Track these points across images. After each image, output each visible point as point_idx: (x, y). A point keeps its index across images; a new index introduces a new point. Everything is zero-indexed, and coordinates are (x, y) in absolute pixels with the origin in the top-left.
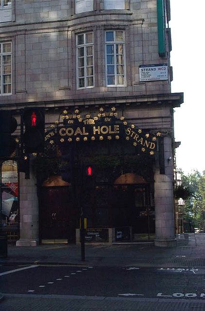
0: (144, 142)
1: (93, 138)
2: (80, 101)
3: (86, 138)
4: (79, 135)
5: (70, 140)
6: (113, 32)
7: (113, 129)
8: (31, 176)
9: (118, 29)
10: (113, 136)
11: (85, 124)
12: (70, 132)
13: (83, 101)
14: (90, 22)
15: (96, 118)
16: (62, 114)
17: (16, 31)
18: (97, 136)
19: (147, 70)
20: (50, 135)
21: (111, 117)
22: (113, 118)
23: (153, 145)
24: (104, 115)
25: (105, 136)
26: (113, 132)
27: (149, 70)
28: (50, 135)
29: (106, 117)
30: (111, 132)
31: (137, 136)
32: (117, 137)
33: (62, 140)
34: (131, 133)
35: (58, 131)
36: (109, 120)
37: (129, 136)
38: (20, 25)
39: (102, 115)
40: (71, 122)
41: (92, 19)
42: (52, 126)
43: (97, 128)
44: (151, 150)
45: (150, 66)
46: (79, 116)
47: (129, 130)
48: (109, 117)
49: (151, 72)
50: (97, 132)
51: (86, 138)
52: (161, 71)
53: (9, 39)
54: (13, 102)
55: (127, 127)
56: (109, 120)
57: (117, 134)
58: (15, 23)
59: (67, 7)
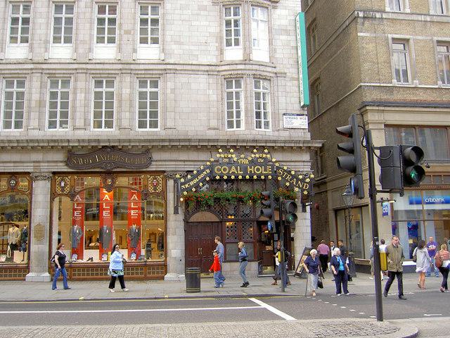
0: (297, 182)
2: (233, 141)
4: (233, 173)
14: (241, 70)
15: (250, 159)
17: (165, 70)
22: (265, 159)
24: (257, 156)
34: (284, 174)
36: (262, 161)
42: (208, 163)
45: (293, 115)
49: (294, 121)
54: (183, 138)
55: (278, 168)
56: (262, 161)
59: (216, 53)
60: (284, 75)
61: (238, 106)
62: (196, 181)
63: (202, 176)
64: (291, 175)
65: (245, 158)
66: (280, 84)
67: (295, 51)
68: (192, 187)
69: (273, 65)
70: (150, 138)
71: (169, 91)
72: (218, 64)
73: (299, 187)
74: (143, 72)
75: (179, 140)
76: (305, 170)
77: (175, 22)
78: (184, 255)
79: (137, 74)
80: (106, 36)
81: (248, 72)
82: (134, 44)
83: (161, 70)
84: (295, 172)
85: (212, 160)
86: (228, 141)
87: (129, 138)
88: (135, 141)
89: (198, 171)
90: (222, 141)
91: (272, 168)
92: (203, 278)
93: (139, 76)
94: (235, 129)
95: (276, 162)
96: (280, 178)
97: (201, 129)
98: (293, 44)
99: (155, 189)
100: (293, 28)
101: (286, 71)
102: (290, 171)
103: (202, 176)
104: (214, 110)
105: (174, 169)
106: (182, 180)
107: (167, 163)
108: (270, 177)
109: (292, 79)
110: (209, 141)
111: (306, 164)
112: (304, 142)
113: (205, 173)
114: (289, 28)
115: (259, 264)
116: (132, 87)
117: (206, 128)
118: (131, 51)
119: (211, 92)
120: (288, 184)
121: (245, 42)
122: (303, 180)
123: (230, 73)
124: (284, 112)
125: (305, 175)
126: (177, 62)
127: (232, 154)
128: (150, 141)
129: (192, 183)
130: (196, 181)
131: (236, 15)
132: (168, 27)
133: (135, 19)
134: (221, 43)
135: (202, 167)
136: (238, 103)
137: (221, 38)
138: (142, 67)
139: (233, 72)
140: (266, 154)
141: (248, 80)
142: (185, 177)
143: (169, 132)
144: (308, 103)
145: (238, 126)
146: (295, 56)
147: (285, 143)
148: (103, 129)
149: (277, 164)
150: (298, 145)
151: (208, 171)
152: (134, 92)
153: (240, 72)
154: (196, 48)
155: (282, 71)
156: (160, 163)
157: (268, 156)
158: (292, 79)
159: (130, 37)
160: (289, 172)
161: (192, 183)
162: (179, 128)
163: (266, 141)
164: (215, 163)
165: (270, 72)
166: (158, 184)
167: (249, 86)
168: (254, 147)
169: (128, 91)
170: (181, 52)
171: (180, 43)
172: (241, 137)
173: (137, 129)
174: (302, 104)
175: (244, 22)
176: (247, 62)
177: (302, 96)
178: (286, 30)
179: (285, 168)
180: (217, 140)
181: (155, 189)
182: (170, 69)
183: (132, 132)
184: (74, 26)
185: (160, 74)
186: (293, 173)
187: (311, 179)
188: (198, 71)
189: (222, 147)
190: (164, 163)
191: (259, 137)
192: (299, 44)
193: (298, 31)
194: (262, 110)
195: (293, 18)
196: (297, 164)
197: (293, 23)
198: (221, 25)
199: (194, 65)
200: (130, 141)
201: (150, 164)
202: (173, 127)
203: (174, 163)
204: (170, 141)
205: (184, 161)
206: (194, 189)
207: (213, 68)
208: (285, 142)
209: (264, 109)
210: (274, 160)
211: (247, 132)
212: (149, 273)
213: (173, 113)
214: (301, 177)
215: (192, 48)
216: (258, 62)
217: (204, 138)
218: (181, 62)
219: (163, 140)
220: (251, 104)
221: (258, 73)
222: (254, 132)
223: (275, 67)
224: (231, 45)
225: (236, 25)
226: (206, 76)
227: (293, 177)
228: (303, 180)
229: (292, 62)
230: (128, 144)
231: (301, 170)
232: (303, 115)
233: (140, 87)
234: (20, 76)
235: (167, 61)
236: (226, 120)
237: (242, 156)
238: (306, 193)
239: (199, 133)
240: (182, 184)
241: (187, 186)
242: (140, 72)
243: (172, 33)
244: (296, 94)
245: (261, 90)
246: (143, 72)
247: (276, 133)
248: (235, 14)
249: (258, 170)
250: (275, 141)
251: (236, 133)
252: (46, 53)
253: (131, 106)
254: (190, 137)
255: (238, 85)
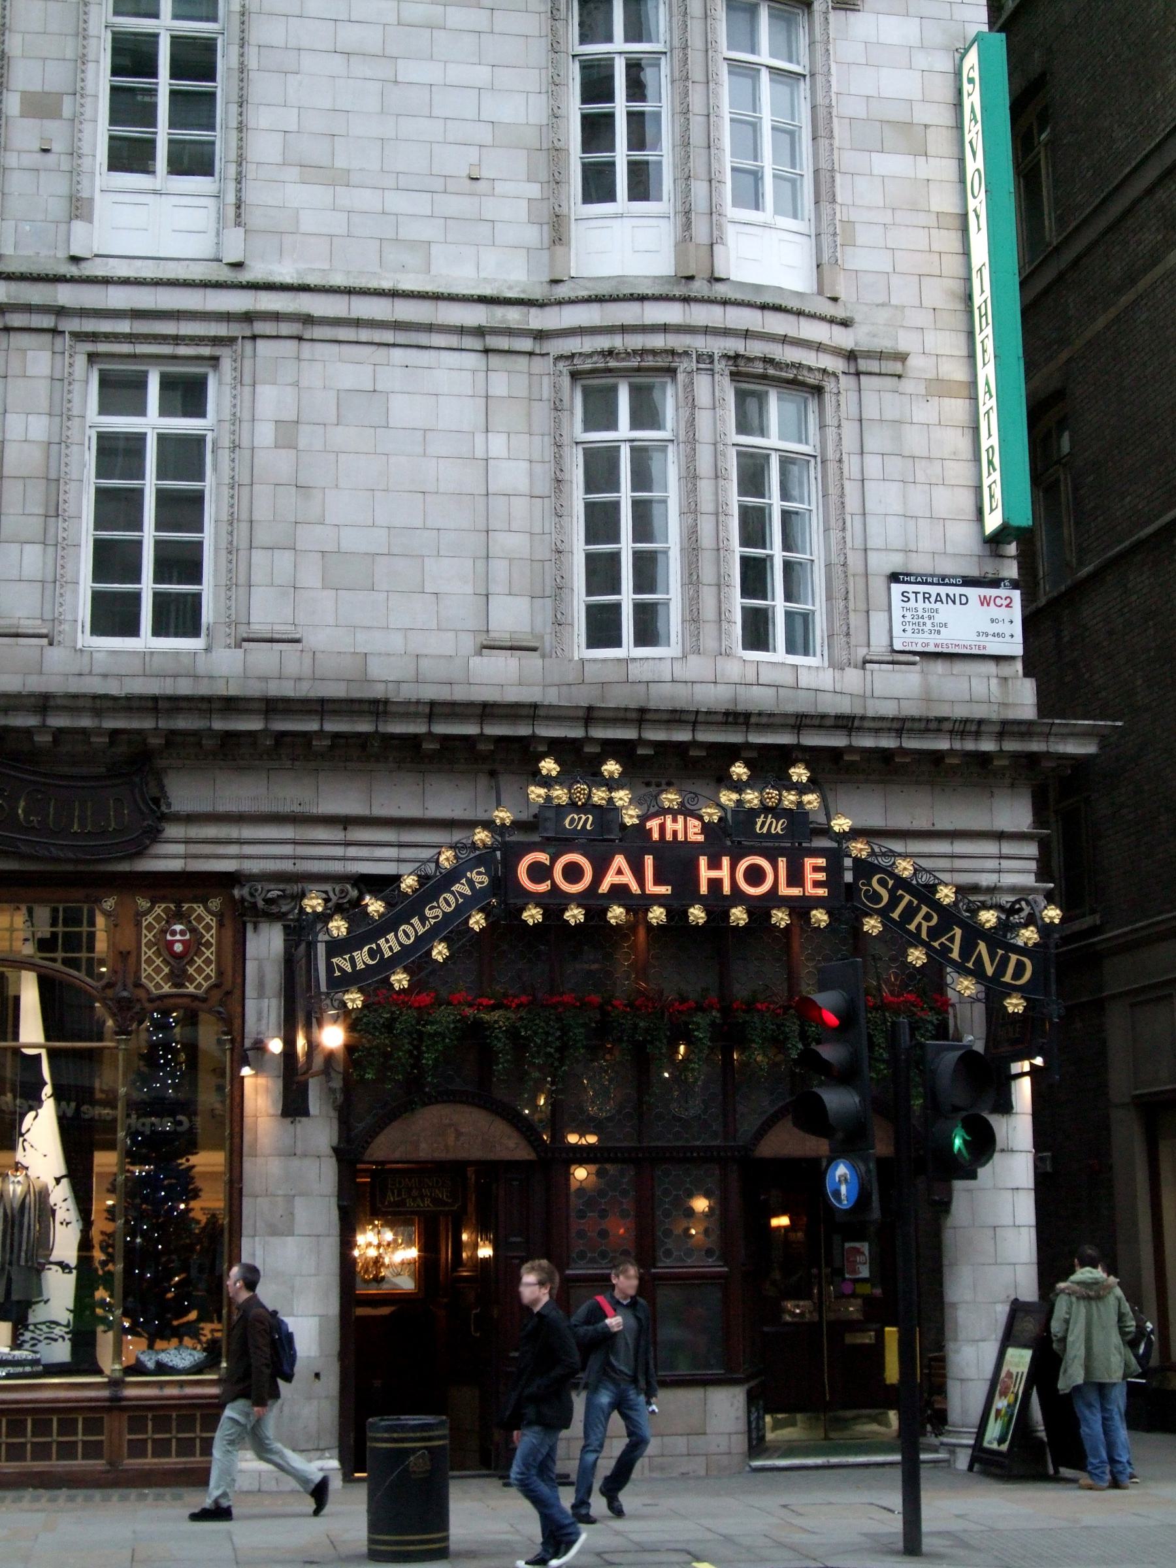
0: (968, 948)
1: (697, 914)
2: (620, 717)
3: (657, 914)
4: (619, 893)
5: (574, 915)
6: (614, 389)
7: (796, 878)
8: (314, 1105)
9: (794, 383)
10: (800, 908)
11: (656, 836)
12: (573, 872)
13: (377, 714)
14: (665, 328)
15: (711, 814)
16: (724, 780)
17: (248, 317)
18: (718, 903)
19: (927, 597)
20: (471, 883)
21: (788, 813)
22: (797, 818)
23: (1020, 966)
24: (752, 797)
25: (760, 909)
26: (796, 891)
27: (938, 598)
28: (471, 883)
29: (765, 809)
30: (784, 891)
31: (927, 917)
32: (820, 917)
33: (533, 915)
34: (894, 901)
35: (510, 866)
36: (778, 827)
37: (884, 914)
38: (106, 281)
39: (548, 798)
40: (586, 821)
41: (671, 314)
42: (481, 836)
43: (714, 864)
44: (1010, 990)
45: (943, 580)
46: (622, 796)
47: (882, 883)
48: (776, 811)
49: (946, 612)
50: (715, 884)
51: (657, 914)
52: (994, 612)
53: (206, 351)
54: (336, 690)
55: (864, 868)
56: (778, 827)
57: (818, 902)
58: (245, 276)
59: (533, 235)
60: (897, 367)
61: (644, 528)
62: (409, 932)
63: (446, 904)
64: (936, 905)
65: (685, 811)
66: (870, 412)
67: (949, 240)
68: (388, 965)
69: (839, 312)
70: (153, 687)
71: (265, 434)
72: (537, 293)
73: (978, 973)
74: (124, 327)
75: (322, 707)
76: (1008, 880)
77: (308, 62)
78: (334, 1345)
79: (94, 337)
80: (163, 133)
81: (700, 343)
82: (74, 173)
83: (227, 317)
84: (960, 890)
85: (503, 816)
86: (590, 716)
87: (35, 684)
88: (75, 703)
89: (423, 879)
90: (555, 715)
91: (833, 870)
92: (454, 1477)
93: (103, 348)
94: (628, 648)
95: (855, 833)
96: (872, 925)
97: (440, 644)
98: (944, 201)
99: (178, 977)
100: (945, 117)
101: (902, 347)
102: (933, 889)
103: (446, 904)
104: (511, 543)
105: (287, 866)
106: (339, 927)
107: (248, 832)
108: (820, 917)
109: (938, 387)
110: (486, 711)
111: (1008, 848)
112: (1007, 728)
113: (462, 888)
114: (923, 114)
115: (751, 1399)
116: (61, 413)
117: (468, 643)
118: (58, 208)
119: (498, 444)
120: (917, 956)
121: (685, 178)
122: (999, 938)
123: (603, 342)
124: (895, 562)
125: (1012, 911)
126: (312, 280)
127: (611, 784)
128: (154, 704)
129: (389, 945)
130: (409, 932)
131: (639, 39)
132: (262, 87)
133: (82, 34)
134: (556, 180)
135: (447, 858)
136: (642, 511)
137: (557, 152)
138: (118, 298)
139: (617, 342)
140: (801, 789)
141: (703, 383)
142: (352, 910)
143: (263, 658)
144: (1024, 518)
145: (647, 633)
146: (953, 265)
147: (97, 713)
148: (146, 641)
149: (859, 848)
150: (970, 745)
151: (480, 878)
152: (74, 434)
153: (658, 341)
154: (421, 204)
155: (884, 343)
156: (211, 831)
157: (811, 800)
158: (938, 387)
159: (55, 130)
160: (926, 893)
161: (389, 945)
162: (317, 639)
163: (801, 722)
164: (516, 837)
165: (819, 347)
166: (195, 945)
167: (704, 420)
168: (732, 753)
169: (39, 427)
170: (336, 223)
171: (337, 178)
172: (663, 697)
173: (87, 640)
174: (993, 522)
175: (683, 80)
176: (699, 287)
177: (992, 480)
178: (906, 127)
179: (905, 868)
180: (531, 712)
181: (178, 977)
182: (276, 317)
183: (56, 657)
184: (223, 86)
185: (216, 341)
186: (946, 895)
187: (1046, 930)
188: (430, 328)
189: (556, 748)
190: (233, 832)
191: (759, 699)
192: (978, 203)
193: (973, 132)
194: (776, 552)
195: (944, 63)
196: (961, 847)
197: (943, 91)
198: (556, 83)
199: (822, 318)
200: (44, 703)
201: (154, 835)
202: (282, 630)
203: (288, 832)
204: (272, 706)
205: (346, 822)
206: (400, 980)
207: (512, 316)
208: (901, 725)
209: (787, 546)
210: (841, 824)
211: (696, 667)
212: (137, 1450)
213: (288, 556)
214: (989, 918)
215: (398, 202)
216: (758, 288)
217: (460, 694)
218: (338, 280)
219: (230, 705)
220: (719, 513)
221: (756, 348)
222: (732, 670)
223: (845, 323)
224: (610, 196)
225: (637, 89)
226: (472, 360)
227: (948, 917)
228: (999, 938)
229: (940, 294)
230: (31, 721)
231: (986, 880)
232: (995, 583)
233: (104, 410)
234: (183, 350)
235: (256, 272)
236: (579, 600)
237: (670, 798)
238: (1015, 1005)
239: (377, 669)
240: (337, 947)
241: (362, 958)
242: (106, 326)
243: (290, 120)
244: (961, 472)
245: (773, 440)
246: (124, 327)
247: (852, 679)
248: (636, 31)
249: (754, 875)
250: (846, 723)
251: (635, 671)
252: (78, 226)
253: (54, 511)
254: (378, 692)
255: (644, 415)
